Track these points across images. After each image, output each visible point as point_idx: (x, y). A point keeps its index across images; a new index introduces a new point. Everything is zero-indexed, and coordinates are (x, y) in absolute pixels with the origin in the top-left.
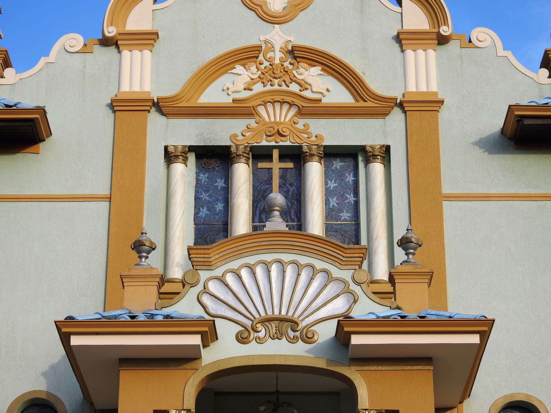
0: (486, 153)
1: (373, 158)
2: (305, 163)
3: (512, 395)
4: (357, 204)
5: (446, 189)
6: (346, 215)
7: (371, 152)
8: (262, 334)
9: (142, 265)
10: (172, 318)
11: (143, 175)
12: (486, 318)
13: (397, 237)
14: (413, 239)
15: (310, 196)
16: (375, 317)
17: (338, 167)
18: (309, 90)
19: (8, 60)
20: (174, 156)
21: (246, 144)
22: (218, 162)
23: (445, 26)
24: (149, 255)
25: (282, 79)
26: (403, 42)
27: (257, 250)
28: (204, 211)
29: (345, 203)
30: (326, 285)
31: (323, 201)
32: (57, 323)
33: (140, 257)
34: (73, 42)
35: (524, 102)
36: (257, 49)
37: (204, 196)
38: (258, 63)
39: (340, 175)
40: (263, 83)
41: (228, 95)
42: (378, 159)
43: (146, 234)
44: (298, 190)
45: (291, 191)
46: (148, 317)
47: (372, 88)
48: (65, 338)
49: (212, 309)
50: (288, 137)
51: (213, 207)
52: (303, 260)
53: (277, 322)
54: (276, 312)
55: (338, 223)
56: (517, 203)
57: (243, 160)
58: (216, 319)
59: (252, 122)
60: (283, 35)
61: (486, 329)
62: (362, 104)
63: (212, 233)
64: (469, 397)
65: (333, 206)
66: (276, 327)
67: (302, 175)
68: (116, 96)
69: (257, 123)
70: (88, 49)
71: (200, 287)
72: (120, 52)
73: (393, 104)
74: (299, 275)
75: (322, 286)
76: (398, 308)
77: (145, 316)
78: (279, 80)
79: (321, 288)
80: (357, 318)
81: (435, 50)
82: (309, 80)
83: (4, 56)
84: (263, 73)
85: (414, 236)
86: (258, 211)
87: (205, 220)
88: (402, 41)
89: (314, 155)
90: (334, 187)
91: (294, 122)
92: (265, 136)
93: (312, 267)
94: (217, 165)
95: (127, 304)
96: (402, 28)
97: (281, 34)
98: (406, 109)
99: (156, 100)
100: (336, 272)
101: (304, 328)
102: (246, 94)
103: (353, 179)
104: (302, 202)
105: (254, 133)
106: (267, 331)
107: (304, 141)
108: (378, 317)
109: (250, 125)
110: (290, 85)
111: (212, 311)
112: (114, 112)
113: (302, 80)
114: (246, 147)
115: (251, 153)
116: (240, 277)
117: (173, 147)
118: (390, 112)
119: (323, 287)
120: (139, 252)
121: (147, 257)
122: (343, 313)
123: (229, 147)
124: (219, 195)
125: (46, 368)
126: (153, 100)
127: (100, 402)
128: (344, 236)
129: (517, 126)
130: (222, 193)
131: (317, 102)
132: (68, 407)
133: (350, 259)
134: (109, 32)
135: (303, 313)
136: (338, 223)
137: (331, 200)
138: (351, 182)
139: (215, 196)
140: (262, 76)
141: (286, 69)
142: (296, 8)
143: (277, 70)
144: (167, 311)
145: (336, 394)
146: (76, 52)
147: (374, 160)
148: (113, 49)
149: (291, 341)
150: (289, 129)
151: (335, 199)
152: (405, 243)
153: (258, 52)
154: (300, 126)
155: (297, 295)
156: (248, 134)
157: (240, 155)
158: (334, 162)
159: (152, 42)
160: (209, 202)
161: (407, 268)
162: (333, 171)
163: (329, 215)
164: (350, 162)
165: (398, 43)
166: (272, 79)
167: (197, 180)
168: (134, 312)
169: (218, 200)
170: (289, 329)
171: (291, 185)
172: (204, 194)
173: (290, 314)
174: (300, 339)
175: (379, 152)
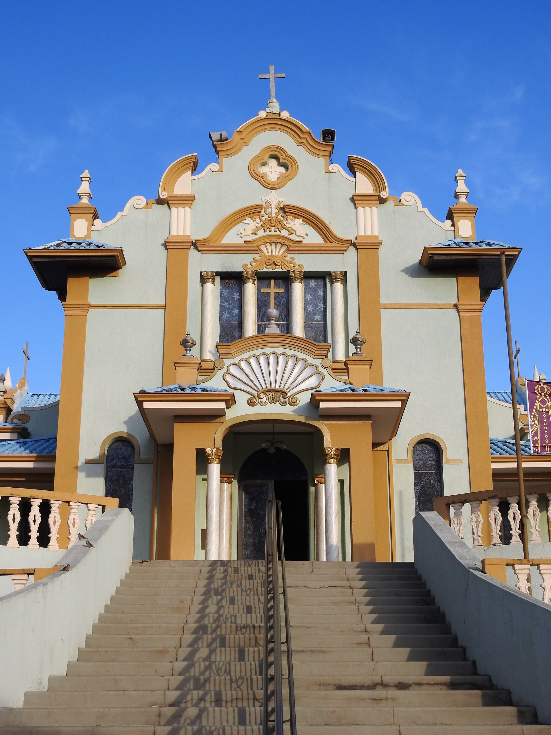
0: (410, 277)
1: (336, 280)
2: (291, 283)
3: (423, 435)
4: (325, 309)
5: (383, 301)
6: (318, 317)
7: (334, 276)
8: (264, 400)
9: (187, 355)
10: (207, 391)
11: (186, 290)
12: (406, 391)
13: (350, 337)
14: (360, 338)
15: (295, 305)
16: (335, 390)
17: (313, 285)
18: (294, 234)
19: (97, 214)
20: (206, 278)
21: (253, 271)
22: (235, 282)
23: (384, 191)
24: (191, 349)
25: (277, 227)
26: (356, 202)
27: (260, 346)
28: (226, 315)
29: (318, 309)
30: (304, 369)
31: (303, 308)
32: (135, 394)
33: (186, 350)
34: (139, 203)
35: (434, 244)
36: (260, 207)
37: (226, 305)
38: (261, 216)
39: (314, 290)
40: (264, 230)
41: (241, 237)
42: (339, 280)
43: (190, 335)
44: (286, 300)
45: (282, 301)
46: (192, 390)
47: (335, 233)
48: (140, 404)
49: (232, 384)
50: (281, 266)
51: (232, 312)
52: (290, 352)
53: (273, 392)
54: (273, 386)
55: (313, 322)
56: (429, 310)
57: (251, 281)
58: (236, 392)
59: (257, 256)
60: (277, 197)
61: (405, 398)
62: (329, 244)
63: (231, 329)
64: (396, 436)
65: (310, 311)
66: (273, 396)
67: (290, 291)
68: (168, 238)
69: (260, 257)
70: (148, 207)
71: (224, 370)
72: (170, 209)
73: (349, 244)
74: (287, 362)
75: (302, 369)
76: (350, 383)
77: (190, 389)
78: (274, 227)
79: (301, 370)
80: (323, 392)
81: (377, 208)
82: (294, 228)
83: (94, 211)
84: (264, 223)
85: (361, 337)
86: (261, 314)
87: (226, 320)
88: (356, 201)
89: (297, 278)
90: (311, 299)
91: (284, 256)
92: (265, 265)
93: (296, 357)
94: (234, 284)
95: (178, 381)
96: (356, 193)
97: (276, 196)
98: (358, 247)
99: (194, 241)
100: (311, 360)
101: (290, 396)
102: (253, 237)
103: (323, 293)
104: (290, 309)
105: (258, 263)
106: (267, 398)
107: (291, 269)
108: (337, 390)
109: (255, 258)
110: (282, 231)
111: (232, 385)
112: (167, 249)
113: (290, 228)
114: (253, 272)
115: (256, 276)
116: (249, 364)
117: (205, 273)
118: (347, 249)
119: (303, 370)
120: (185, 347)
121: (190, 350)
122: (315, 387)
123: (242, 273)
124: (235, 304)
125: (126, 418)
126: (192, 241)
127: (161, 439)
128: (317, 331)
129: (430, 260)
130: (238, 302)
131: (299, 243)
132: (140, 442)
133: (319, 352)
134: (163, 196)
135: (289, 387)
136: (313, 322)
137: (308, 307)
138: (321, 295)
139: (233, 305)
140: (263, 225)
141: (279, 221)
142: (286, 178)
143: (273, 221)
144: (204, 385)
145: (311, 434)
146: (141, 209)
147: (336, 282)
148: (165, 206)
149: (282, 405)
150: (281, 261)
151: (311, 307)
152: (355, 341)
153: (261, 209)
154: (288, 258)
155: (286, 375)
156: (254, 264)
157: (249, 278)
158: (311, 282)
159: (191, 202)
160: (229, 309)
161: (356, 358)
162: (310, 288)
163: (307, 317)
164: (320, 282)
165: (353, 203)
166: (270, 227)
167: (221, 294)
168: (183, 386)
169: (235, 307)
170: (281, 396)
171: (282, 297)
172: (226, 303)
173: (282, 387)
174: (288, 403)
175: (340, 276)
